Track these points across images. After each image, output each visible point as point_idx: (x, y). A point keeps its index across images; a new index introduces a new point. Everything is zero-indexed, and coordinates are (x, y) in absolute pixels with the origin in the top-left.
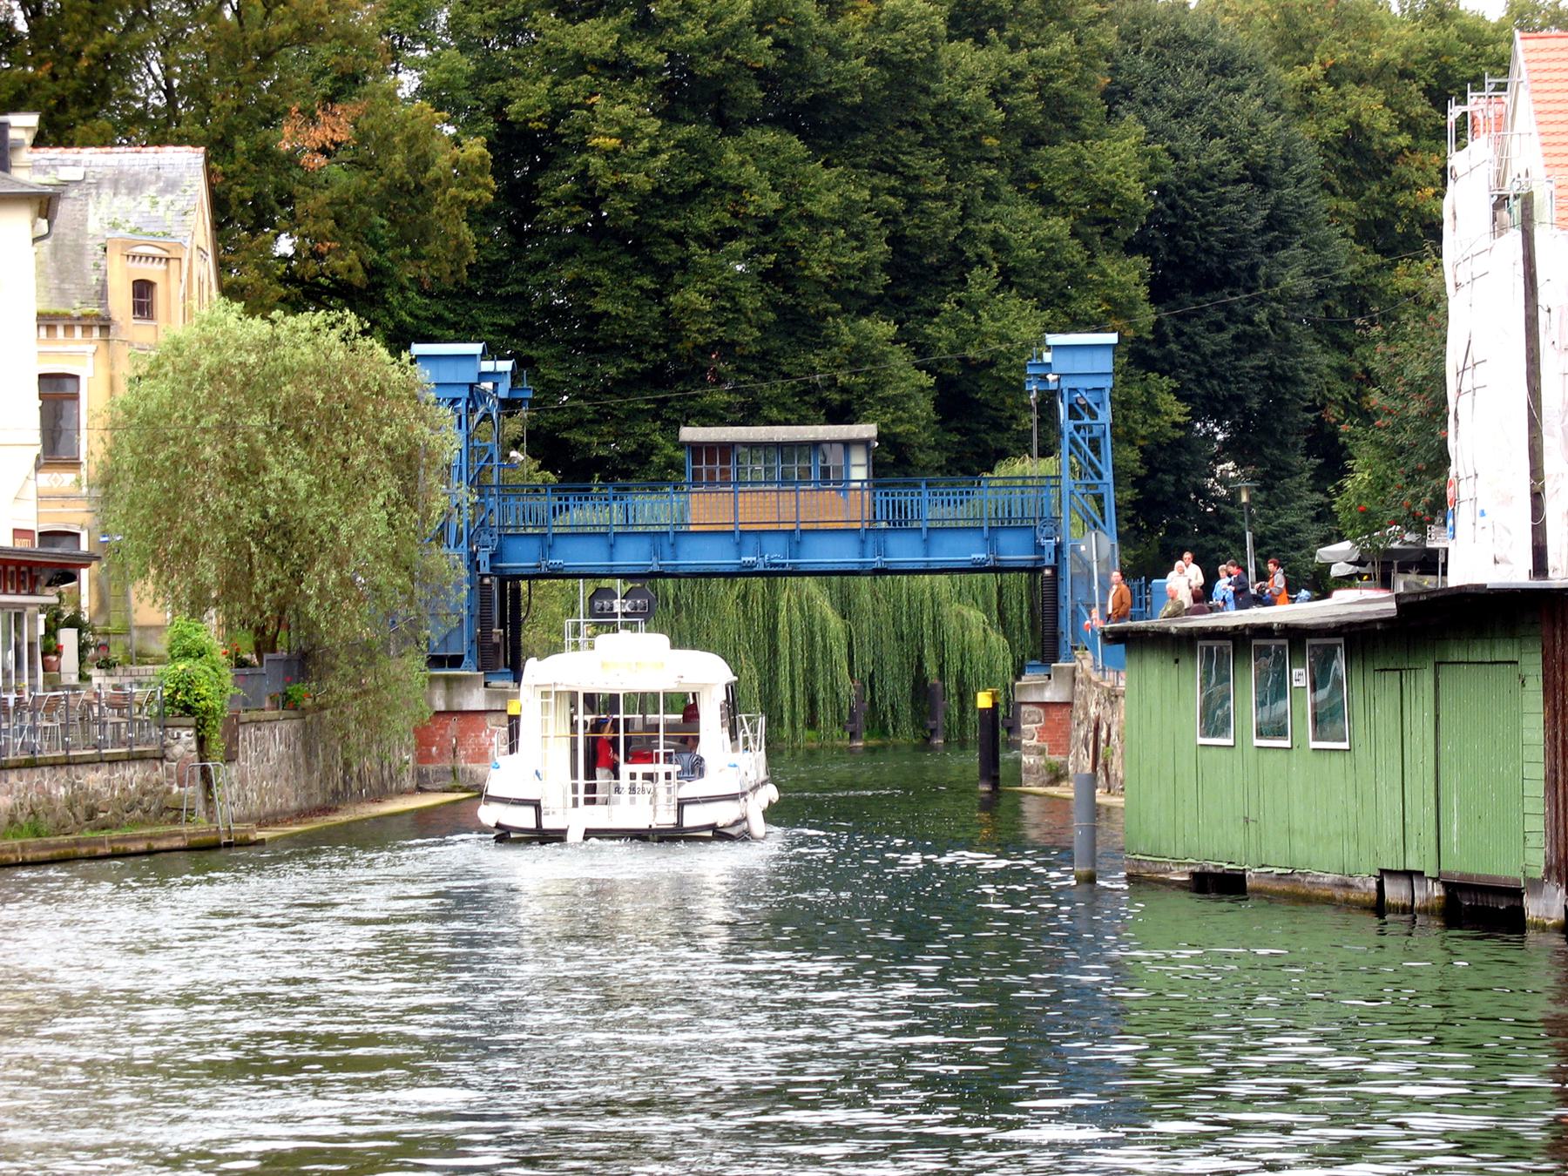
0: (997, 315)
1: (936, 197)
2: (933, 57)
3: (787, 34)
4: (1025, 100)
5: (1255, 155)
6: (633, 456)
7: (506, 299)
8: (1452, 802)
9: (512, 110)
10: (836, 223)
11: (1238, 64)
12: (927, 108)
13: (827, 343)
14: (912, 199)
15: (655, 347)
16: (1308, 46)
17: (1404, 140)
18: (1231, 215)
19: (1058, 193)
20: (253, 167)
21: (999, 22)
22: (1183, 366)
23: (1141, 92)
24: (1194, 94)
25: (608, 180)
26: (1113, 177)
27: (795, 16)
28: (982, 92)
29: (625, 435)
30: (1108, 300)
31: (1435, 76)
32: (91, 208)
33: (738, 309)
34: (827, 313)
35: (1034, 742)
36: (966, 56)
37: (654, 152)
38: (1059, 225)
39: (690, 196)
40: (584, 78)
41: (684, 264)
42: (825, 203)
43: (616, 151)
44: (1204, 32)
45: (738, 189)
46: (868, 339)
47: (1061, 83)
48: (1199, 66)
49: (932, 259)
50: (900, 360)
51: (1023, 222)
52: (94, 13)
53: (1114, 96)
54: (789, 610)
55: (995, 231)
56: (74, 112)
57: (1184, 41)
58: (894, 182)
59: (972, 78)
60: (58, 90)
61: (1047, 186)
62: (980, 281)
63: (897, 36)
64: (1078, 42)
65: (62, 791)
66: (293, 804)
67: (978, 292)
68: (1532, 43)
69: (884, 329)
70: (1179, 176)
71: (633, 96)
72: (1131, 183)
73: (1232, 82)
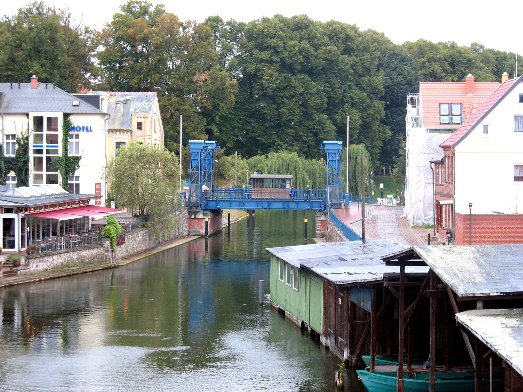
0: (350, 113)
1: (338, 88)
2: (337, 59)
3: (306, 55)
4: (359, 69)
5: (409, 79)
6: (272, 143)
7: (245, 109)
8: (312, 310)
9: (248, 70)
10: (316, 94)
11: (406, 59)
12: (336, 69)
13: (313, 120)
14: (333, 89)
15: (277, 120)
16: (424, 53)
17: (444, 74)
18: (403, 92)
19: (365, 87)
20: (189, 84)
21: (354, 51)
22: (392, 123)
23: (385, 65)
24: (397, 66)
25: (266, 86)
26: (377, 84)
27: (308, 51)
28: (349, 66)
29: (270, 139)
30: (375, 110)
31: (451, 60)
32: (132, 106)
33: (294, 112)
34: (314, 113)
35: (319, 228)
36: (347, 59)
37: (277, 79)
38: (365, 94)
39: (285, 88)
40: (263, 64)
41: (283, 103)
42: (314, 90)
43: (269, 79)
44: (399, 52)
45: (295, 87)
46: (321, 119)
47: (366, 64)
48: (398, 60)
49: (337, 101)
50: (329, 123)
51: (357, 94)
52: (157, 52)
53: (378, 67)
54: (299, 178)
55: (350, 95)
56: (152, 72)
57: (395, 54)
58: (329, 85)
59: (347, 63)
60: (149, 67)
61: (363, 86)
62: (347, 106)
63: (330, 55)
64: (371, 55)
65: (76, 257)
66: (144, 248)
67: (346, 109)
68: (423, 85)
69: (324, 117)
70: (392, 83)
71: (273, 67)
72: (381, 86)
73: (405, 63)
